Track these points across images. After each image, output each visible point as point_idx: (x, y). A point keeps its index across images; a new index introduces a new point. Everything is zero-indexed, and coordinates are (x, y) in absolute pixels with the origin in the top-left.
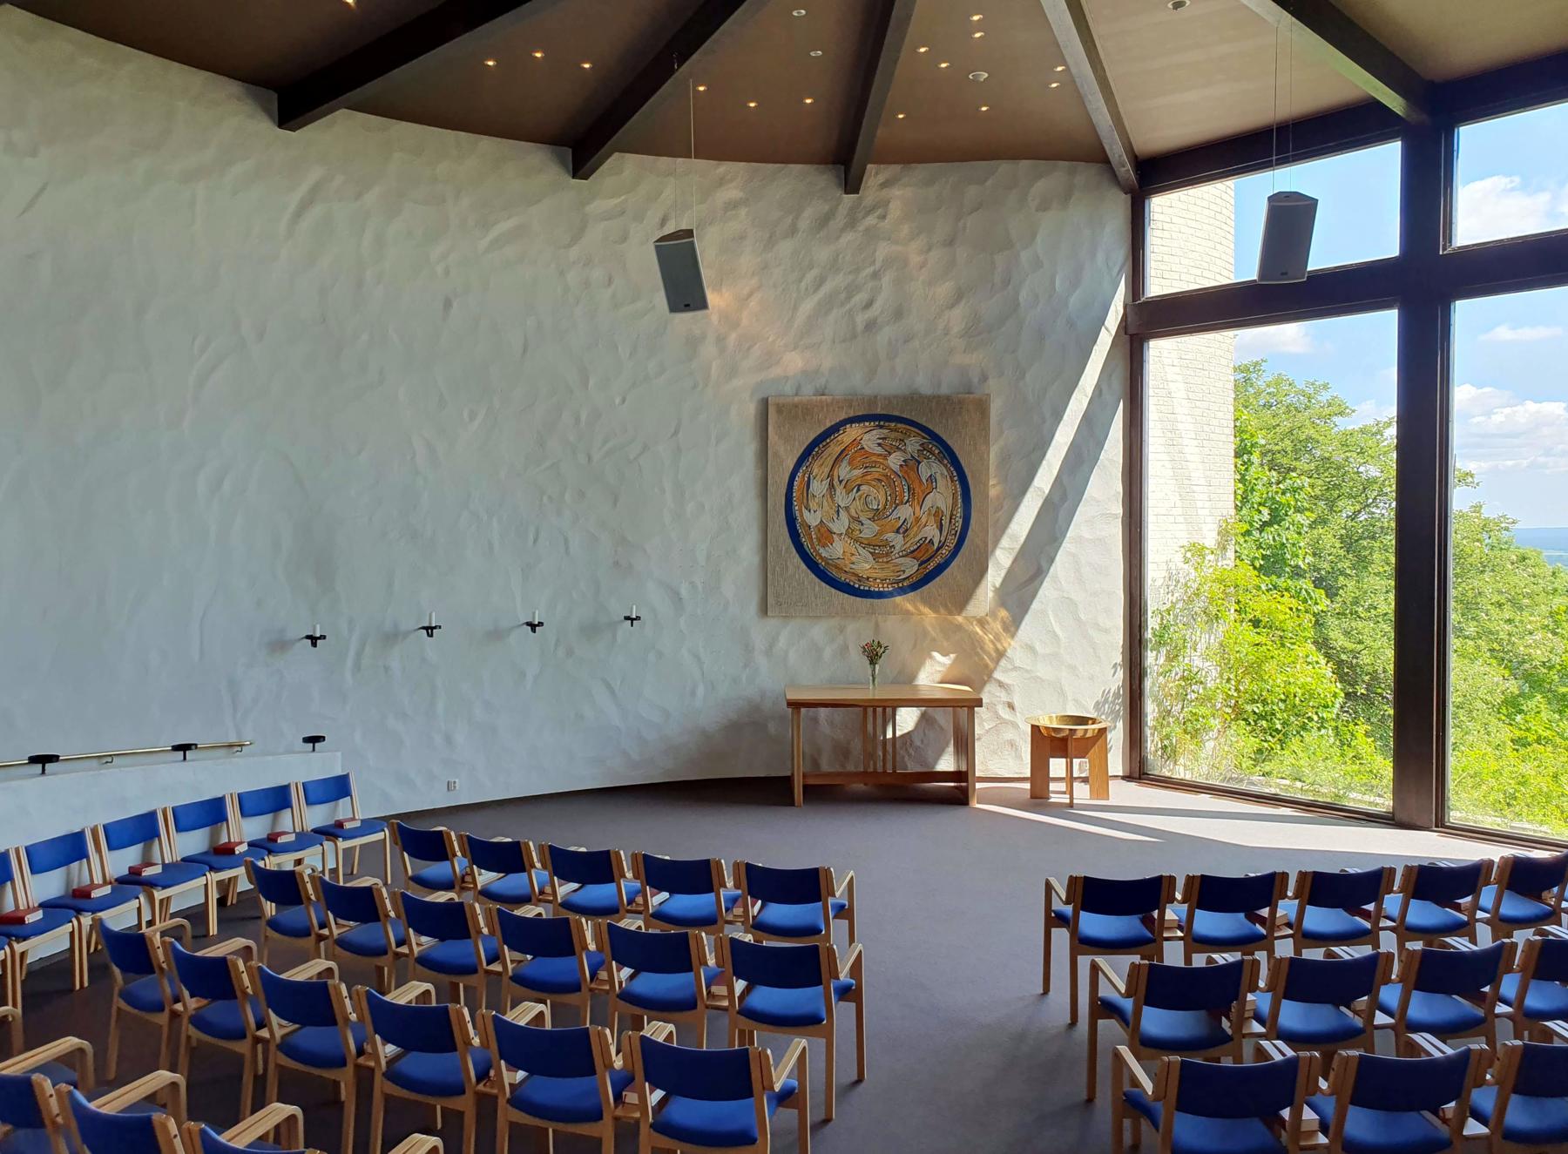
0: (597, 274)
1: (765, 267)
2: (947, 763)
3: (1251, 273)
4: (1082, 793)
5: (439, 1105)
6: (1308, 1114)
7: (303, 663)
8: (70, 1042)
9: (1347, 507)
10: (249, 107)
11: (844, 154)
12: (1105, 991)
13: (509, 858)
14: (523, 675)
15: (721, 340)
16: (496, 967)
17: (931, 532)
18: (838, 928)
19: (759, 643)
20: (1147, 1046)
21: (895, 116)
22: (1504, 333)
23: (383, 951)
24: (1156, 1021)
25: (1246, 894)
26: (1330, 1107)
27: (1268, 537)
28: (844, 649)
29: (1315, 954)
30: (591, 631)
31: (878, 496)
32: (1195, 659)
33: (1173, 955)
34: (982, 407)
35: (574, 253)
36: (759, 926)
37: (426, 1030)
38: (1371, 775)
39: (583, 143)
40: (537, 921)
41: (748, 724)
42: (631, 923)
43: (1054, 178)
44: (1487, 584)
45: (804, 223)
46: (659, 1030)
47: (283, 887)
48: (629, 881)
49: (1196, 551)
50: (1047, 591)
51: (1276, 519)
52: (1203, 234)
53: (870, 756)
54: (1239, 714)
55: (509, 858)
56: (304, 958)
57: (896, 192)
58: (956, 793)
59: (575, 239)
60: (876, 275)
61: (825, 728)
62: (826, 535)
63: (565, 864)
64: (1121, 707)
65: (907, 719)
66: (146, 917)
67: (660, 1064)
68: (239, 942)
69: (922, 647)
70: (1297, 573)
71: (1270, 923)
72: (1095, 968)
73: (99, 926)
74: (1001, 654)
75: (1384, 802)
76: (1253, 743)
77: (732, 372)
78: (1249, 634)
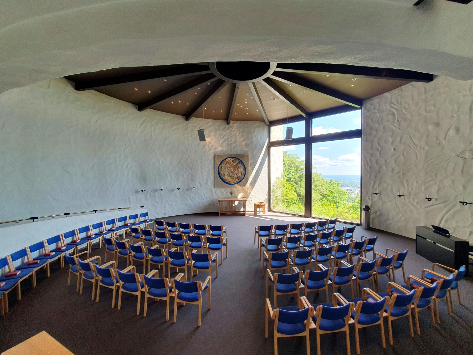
0: (189, 135)
1: (215, 135)
2: (242, 210)
3: (285, 139)
4: (262, 213)
5: (160, 265)
6: (290, 260)
7: (141, 195)
8: (97, 257)
9: (299, 172)
10: (133, 107)
11: (227, 119)
12: (262, 243)
13: (173, 225)
14: (177, 197)
15: (208, 145)
16: (170, 242)
17: (240, 175)
18: (224, 234)
19: (214, 192)
20: (268, 250)
21: (234, 114)
22: (321, 148)
23: (151, 240)
24: (270, 247)
25: (282, 228)
26: (293, 258)
27: (288, 176)
28: (227, 192)
29: (292, 236)
30: (188, 190)
31: (232, 169)
32: (277, 194)
33: (273, 237)
34: (247, 156)
35: (186, 132)
36: (212, 235)
37: (157, 253)
38: (301, 210)
39: (187, 115)
40: (177, 235)
41: (212, 204)
42: (192, 235)
43: (257, 124)
44: (318, 183)
45: (221, 128)
46: (195, 251)
47: (135, 231)
48: (192, 228)
49: (278, 178)
50: (257, 184)
51: (289, 173)
52: (278, 132)
53: (231, 209)
54: (284, 202)
55: (173, 225)
56: (138, 242)
57: (235, 125)
58: (243, 214)
59: (186, 130)
60: (232, 137)
61: (224, 204)
62: (224, 175)
63: (182, 226)
64: (267, 201)
65: (236, 203)
66: (113, 236)
67: (194, 257)
68: (127, 240)
69: (239, 192)
70: (292, 181)
71: (286, 232)
72: (261, 239)
73: (103, 237)
74: (250, 193)
75: (303, 214)
76: (286, 206)
77: (210, 150)
78: (285, 190)
